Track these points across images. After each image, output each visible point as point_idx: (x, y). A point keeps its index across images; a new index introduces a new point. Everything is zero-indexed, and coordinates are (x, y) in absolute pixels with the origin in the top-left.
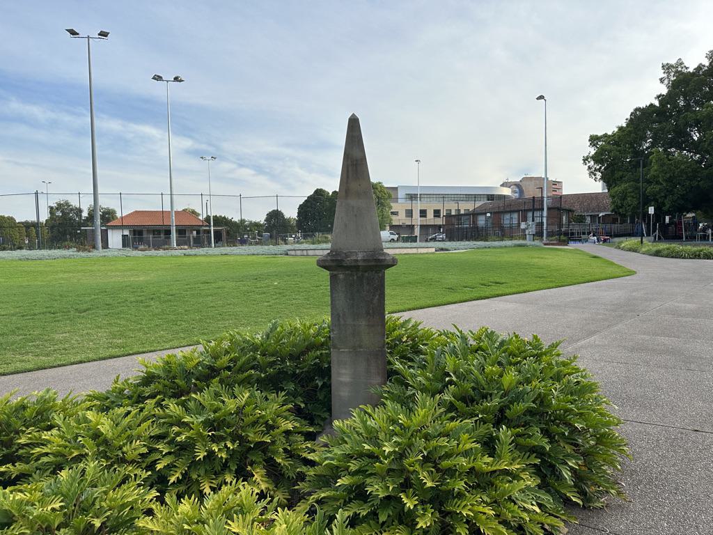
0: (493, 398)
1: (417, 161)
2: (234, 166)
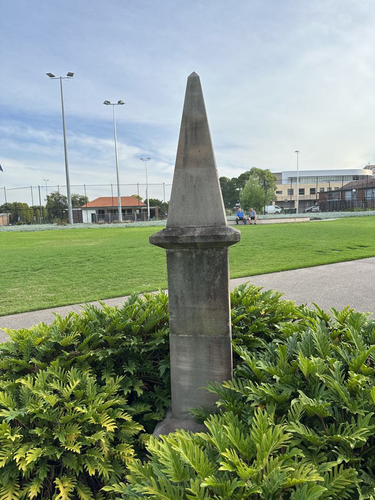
0: (359, 424)
1: (296, 152)
2: (166, 164)
